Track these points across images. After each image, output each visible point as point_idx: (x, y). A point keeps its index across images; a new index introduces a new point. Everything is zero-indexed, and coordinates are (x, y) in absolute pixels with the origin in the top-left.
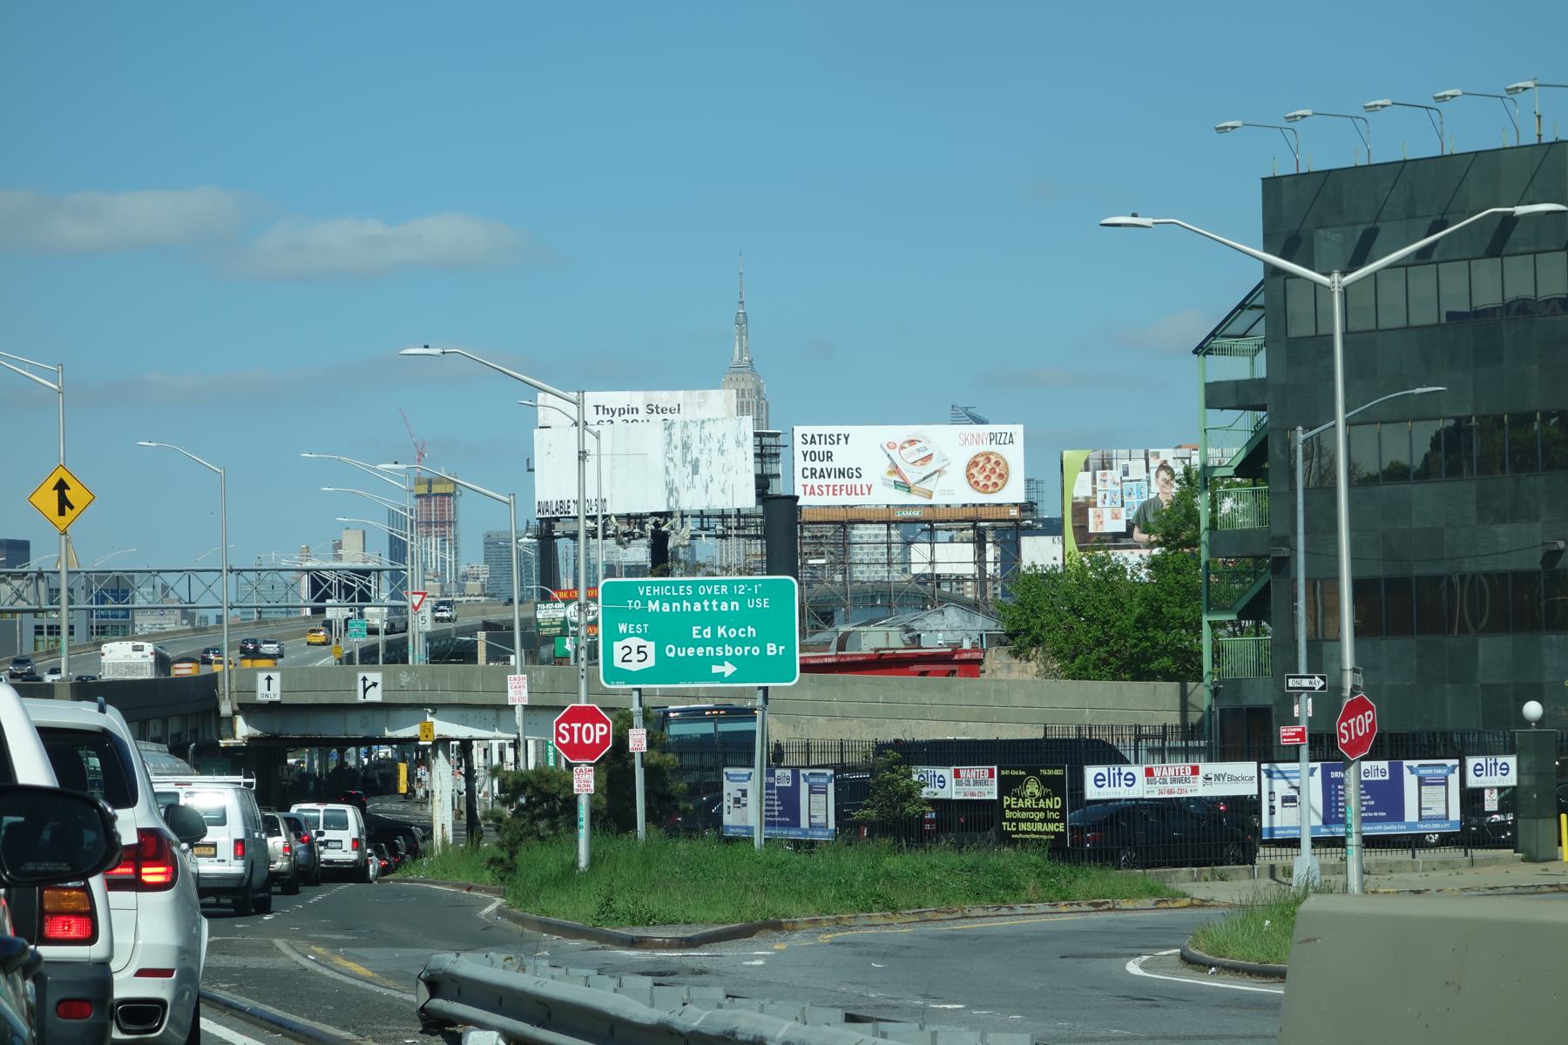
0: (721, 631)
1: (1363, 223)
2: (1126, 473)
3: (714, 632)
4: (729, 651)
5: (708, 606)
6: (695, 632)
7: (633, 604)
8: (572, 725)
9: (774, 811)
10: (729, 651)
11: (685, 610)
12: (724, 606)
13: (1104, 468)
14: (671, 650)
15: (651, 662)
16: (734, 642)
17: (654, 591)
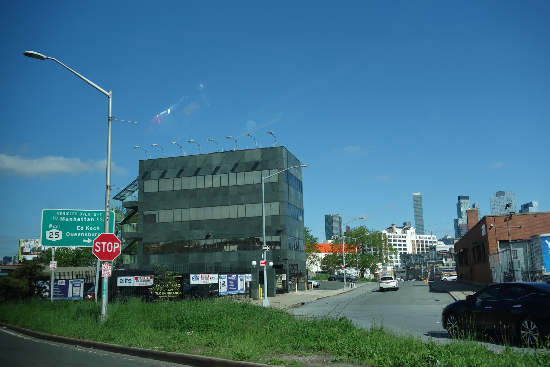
0: (87, 228)
1: (164, 169)
2: (30, 243)
3: (85, 228)
4: (90, 235)
5: (86, 220)
6: (77, 228)
7: (55, 218)
8: (102, 243)
9: (57, 292)
10: (90, 235)
11: (74, 220)
12: (89, 220)
13: (27, 242)
14: (68, 234)
15: (60, 238)
16: (92, 232)
17: (63, 214)
